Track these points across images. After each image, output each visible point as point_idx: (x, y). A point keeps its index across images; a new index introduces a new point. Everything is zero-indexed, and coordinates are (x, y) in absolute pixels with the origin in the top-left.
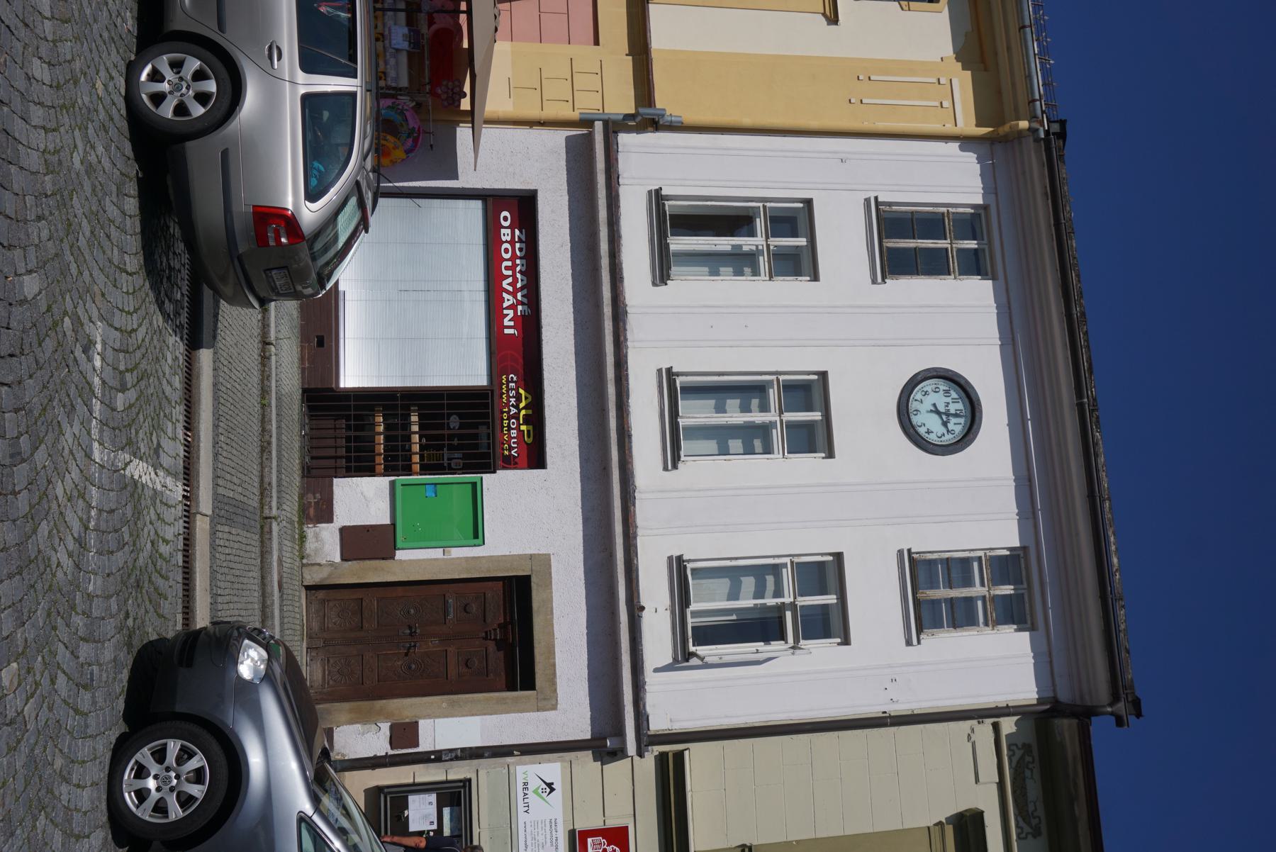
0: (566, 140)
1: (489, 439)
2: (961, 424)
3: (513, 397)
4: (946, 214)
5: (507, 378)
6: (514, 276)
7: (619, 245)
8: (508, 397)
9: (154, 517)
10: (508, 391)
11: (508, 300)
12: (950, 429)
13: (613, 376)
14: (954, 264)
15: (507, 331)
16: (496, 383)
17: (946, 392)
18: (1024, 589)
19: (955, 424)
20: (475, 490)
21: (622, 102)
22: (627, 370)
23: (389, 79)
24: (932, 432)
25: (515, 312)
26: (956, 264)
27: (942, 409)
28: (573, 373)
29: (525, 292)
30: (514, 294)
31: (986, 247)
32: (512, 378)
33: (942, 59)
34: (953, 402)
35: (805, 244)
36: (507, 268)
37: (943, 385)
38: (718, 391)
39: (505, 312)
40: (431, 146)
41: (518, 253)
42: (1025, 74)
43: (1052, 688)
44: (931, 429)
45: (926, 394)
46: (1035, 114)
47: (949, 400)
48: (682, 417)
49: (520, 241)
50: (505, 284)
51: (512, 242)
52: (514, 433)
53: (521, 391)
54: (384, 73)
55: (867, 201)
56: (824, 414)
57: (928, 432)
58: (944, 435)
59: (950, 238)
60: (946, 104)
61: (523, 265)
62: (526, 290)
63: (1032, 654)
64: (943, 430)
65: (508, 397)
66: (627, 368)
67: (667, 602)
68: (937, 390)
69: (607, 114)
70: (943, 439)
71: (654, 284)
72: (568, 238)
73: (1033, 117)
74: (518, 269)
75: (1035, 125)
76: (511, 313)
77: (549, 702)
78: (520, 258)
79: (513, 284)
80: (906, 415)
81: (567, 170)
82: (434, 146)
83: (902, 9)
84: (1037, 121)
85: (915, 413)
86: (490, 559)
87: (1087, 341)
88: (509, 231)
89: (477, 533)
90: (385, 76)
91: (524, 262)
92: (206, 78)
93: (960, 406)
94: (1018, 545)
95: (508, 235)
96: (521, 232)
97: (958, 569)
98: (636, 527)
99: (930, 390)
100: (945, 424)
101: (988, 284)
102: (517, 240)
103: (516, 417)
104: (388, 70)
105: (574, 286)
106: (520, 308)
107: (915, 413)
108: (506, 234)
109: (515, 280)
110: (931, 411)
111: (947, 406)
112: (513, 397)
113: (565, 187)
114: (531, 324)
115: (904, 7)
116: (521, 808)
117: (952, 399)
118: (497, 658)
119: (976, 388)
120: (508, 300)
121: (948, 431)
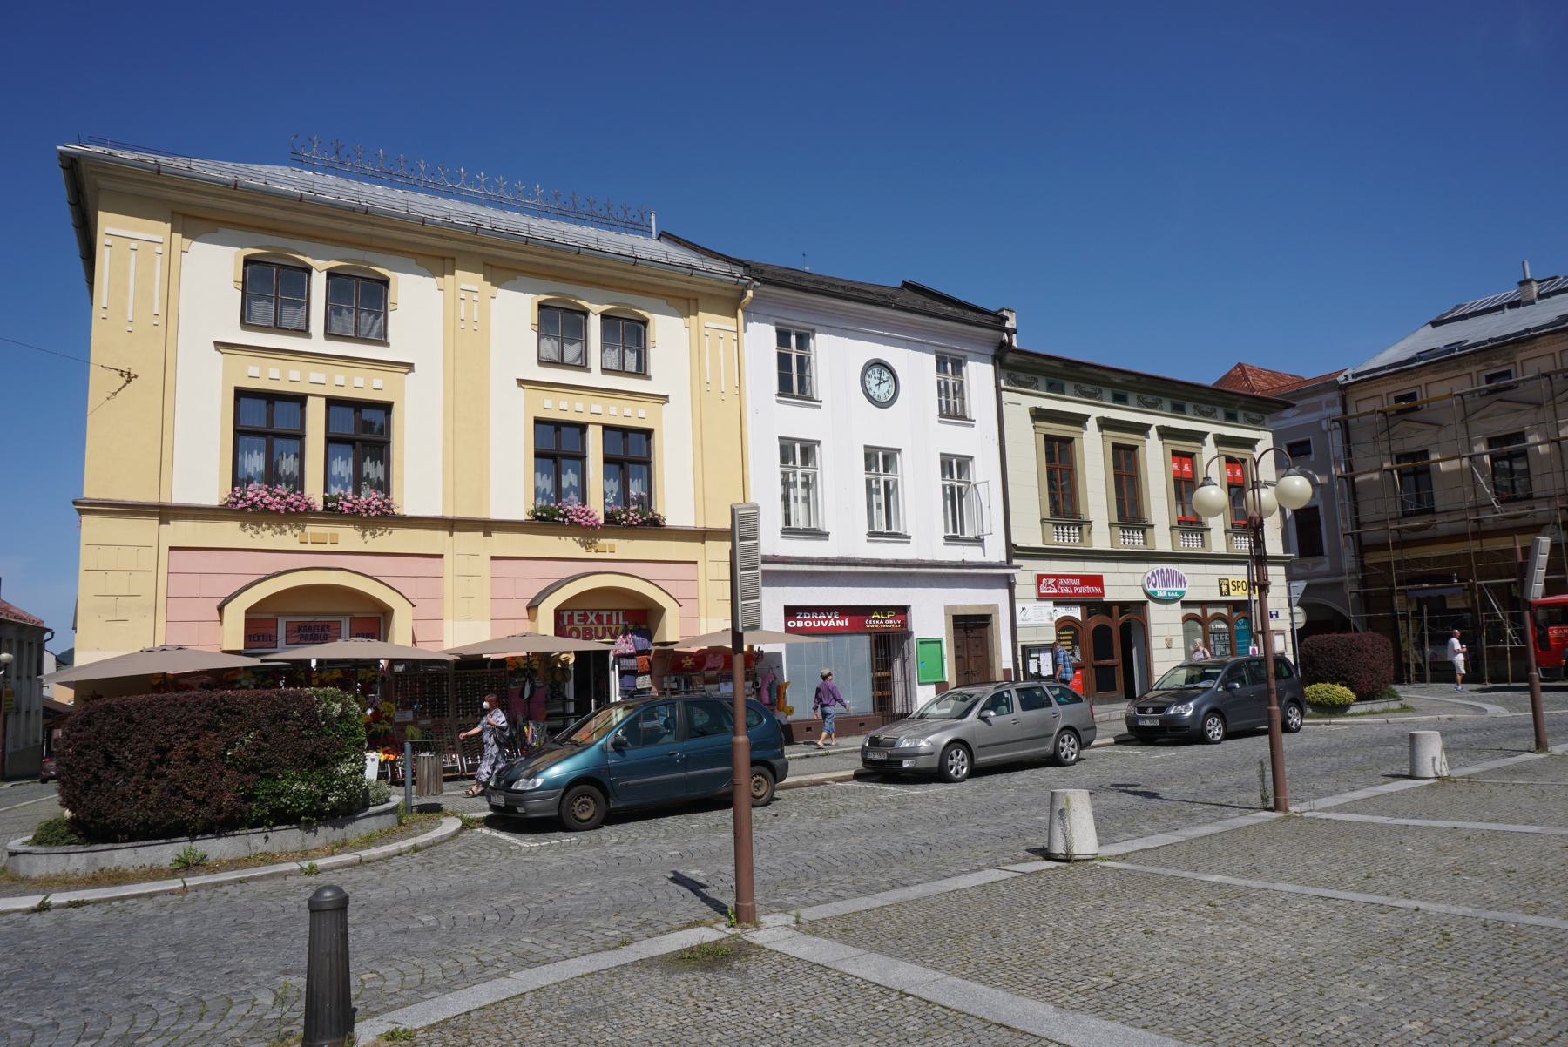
11: (832, 623)
20: (923, 642)
27: (877, 382)
28: (871, 589)
30: (829, 620)
50: (824, 625)
51: (804, 620)
52: (891, 622)
67: (960, 547)
76: (838, 622)
77: (995, 607)
79: (824, 620)
86: (947, 635)
89: (939, 642)
93: (876, 370)
103: (884, 620)
108: (800, 624)
114: (843, 611)
116: (1029, 622)
118: (977, 632)
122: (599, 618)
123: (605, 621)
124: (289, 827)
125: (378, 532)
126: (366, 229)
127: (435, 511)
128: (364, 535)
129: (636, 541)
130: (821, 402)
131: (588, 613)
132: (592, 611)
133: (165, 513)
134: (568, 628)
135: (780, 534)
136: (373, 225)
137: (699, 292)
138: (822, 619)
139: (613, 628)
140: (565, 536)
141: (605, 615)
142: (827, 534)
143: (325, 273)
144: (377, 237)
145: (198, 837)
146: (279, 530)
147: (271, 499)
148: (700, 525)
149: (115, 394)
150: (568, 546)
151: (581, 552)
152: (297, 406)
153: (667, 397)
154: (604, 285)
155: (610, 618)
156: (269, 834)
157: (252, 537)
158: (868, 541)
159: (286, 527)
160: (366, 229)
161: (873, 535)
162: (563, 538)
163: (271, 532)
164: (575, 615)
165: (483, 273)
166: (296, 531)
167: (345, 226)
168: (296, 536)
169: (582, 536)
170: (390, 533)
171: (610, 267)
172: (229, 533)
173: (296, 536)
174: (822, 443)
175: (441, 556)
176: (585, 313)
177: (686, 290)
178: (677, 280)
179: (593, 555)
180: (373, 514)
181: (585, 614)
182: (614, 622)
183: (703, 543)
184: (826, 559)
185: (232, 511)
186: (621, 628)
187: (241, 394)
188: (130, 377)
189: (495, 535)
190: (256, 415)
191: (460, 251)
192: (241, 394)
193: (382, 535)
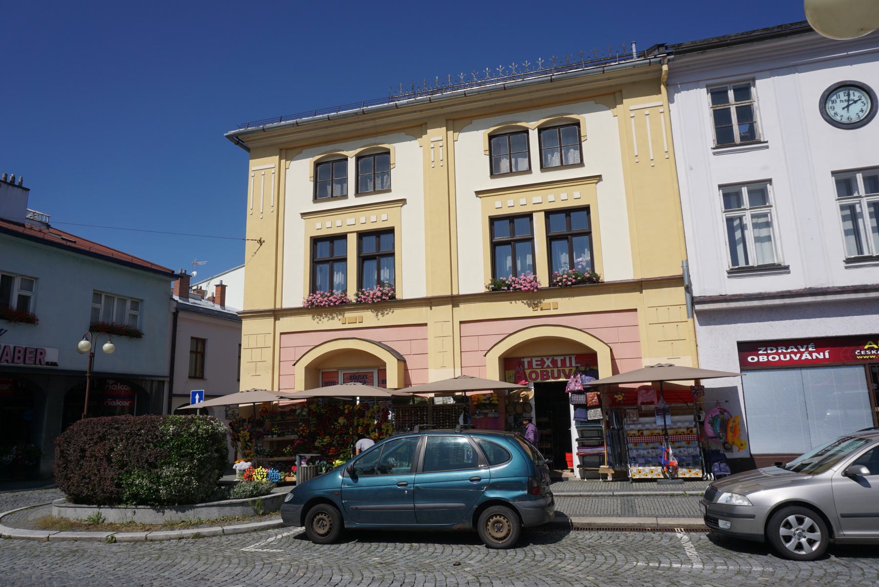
0: (702, 326)
1: (875, 366)
2: (854, 93)
3: (871, 352)
4: (714, 109)
5: (859, 356)
6: (790, 353)
7: (765, 294)
8: (871, 354)
9: (581, 541)
10: (868, 355)
11: (806, 356)
12: (858, 99)
13: (863, 294)
14: (745, 103)
15: (827, 356)
16: (863, 362)
17: (833, 102)
18: (730, 86)
19: (854, 96)
21: (678, 294)
22: (849, 287)
23: (690, 426)
24: (862, 109)
25: (814, 352)
26: (746, 101)
27: (846, 104)
29: (799, 347)
30: (802, 353)
31: (732, 85)
32: (858, 353)
33: (420, 147)
34: (839, 98)
35: (746, 188)
36: (785, 357)
37: (829, 104)
38: (735, 243)
39: (814, 358)
40: (726, 401)
41: (774, 351)
42: (477, 94)
43: (792, 67)
44: (860, 109)
45: (836, 114)
46: (658, 61)
47: (838, 100)
48: (872, 254)
49: (766, 350)
51: (768, 355)
53: (866, 347)
54: (639, 431)
55: (714, 154)
56: (743, 185)
57: (862, 111)
58: (863, 102)
59: (729, 105)
60: (647, 112)
61: (782, 348)
62: (798, 346)
63: (772, 77)
64: (859, 103)
65: (871, 354)
66: (848, 286)
68: (832, 107)
69: (687, 302)
70: (865, 102)
71: (789, 273)
72: (765, 323)
73: (661, 63)
74: (785, 351)
75: (666, 61)
78: (777, 350)
79: (795, 354)
80: (855, 124)
81: (721, 325)
82: (726, 400)
83: (586, 140)
84: (663, 60)
85: (850, 119)
87: (796, 24)
88: (761, 357)
90: (690, 428)
91: (779, 348)
92: (784, 537)
93: (841, 94)
94: (706, 89)
95: (763, 360)
96: (760, 350)
97: (721, 119)
98: (805, 288)
99: (833, 112)
100: (855, 102)
101: (758, 82)
102: (766, 352)
104: (637, 428)
105: (715, 324)
106: (810, 349)
107: (850, 119)
109: (792, 352)
110: (848, 110)
111: (843, 101)
112: (871, 352)
113: (733, 326)
114: (820, 343)
115: (585, 139)
117: (837, 98)
119: (831, 85)
120: (806, 356)
121: (860, 100)
122: (554, 363)
123: (559, 364)
124: (145, 507)
125: (386, 312)
126: (371, 123)
127: (629, 275)
128: (377, 315)
129: (576, 298)
130: (767, 142)
131: (545, 359)
132: (548, 357)
133: (455, 300)
134: (528, 372)
135: (726, 274)
136: (374, 119)
137: (621, 85)
138: (792, 352)
139: (567, 370)
140: (515, 300)
141: (559, 359)
142: (787, 268)
143: (537, 130)
144: (380, 126)
145: (102, 506)
146: (331, 317)
147: (322, 299)
148: (639, 277)
149: (255, 253)
150: (519, 308)
151: (530, 312)
152: (585, 213)
153: (600, 176)
154: (539, 106)
155: (563, 362)
156: (136, 510)
157: (318, 323)
158: (846, 268)
159: (335, 315)
160: (371, 123)
161: (850, 262)
162: (513, 302)
163: (327, 319)
164: (534, 360)
165: (675, 93)
166: (340, 317)
167: (360, 126)
168: (340, 320)
169: (529, 299)
170: (393, 312)
171: (537, 91)
172: (307, 322)
173: (340, 320)
174: (773, 181)
175: (426, 325)
176: (526, 131)
177: (610, 86)
178: (786, 54)
179: (539, 313)
180: (376, 301)
181: (542, 359)
182: (568, 364)
183: (641, 292)
184: (760, 294)
185: (312, 308)
186: (574, 369)
187: (493, 220)
188: (261, 242)
189: (462, 306)
190: (324, 251)
191: (430, 117)
192: (493, 220)
193: (387, 314)
